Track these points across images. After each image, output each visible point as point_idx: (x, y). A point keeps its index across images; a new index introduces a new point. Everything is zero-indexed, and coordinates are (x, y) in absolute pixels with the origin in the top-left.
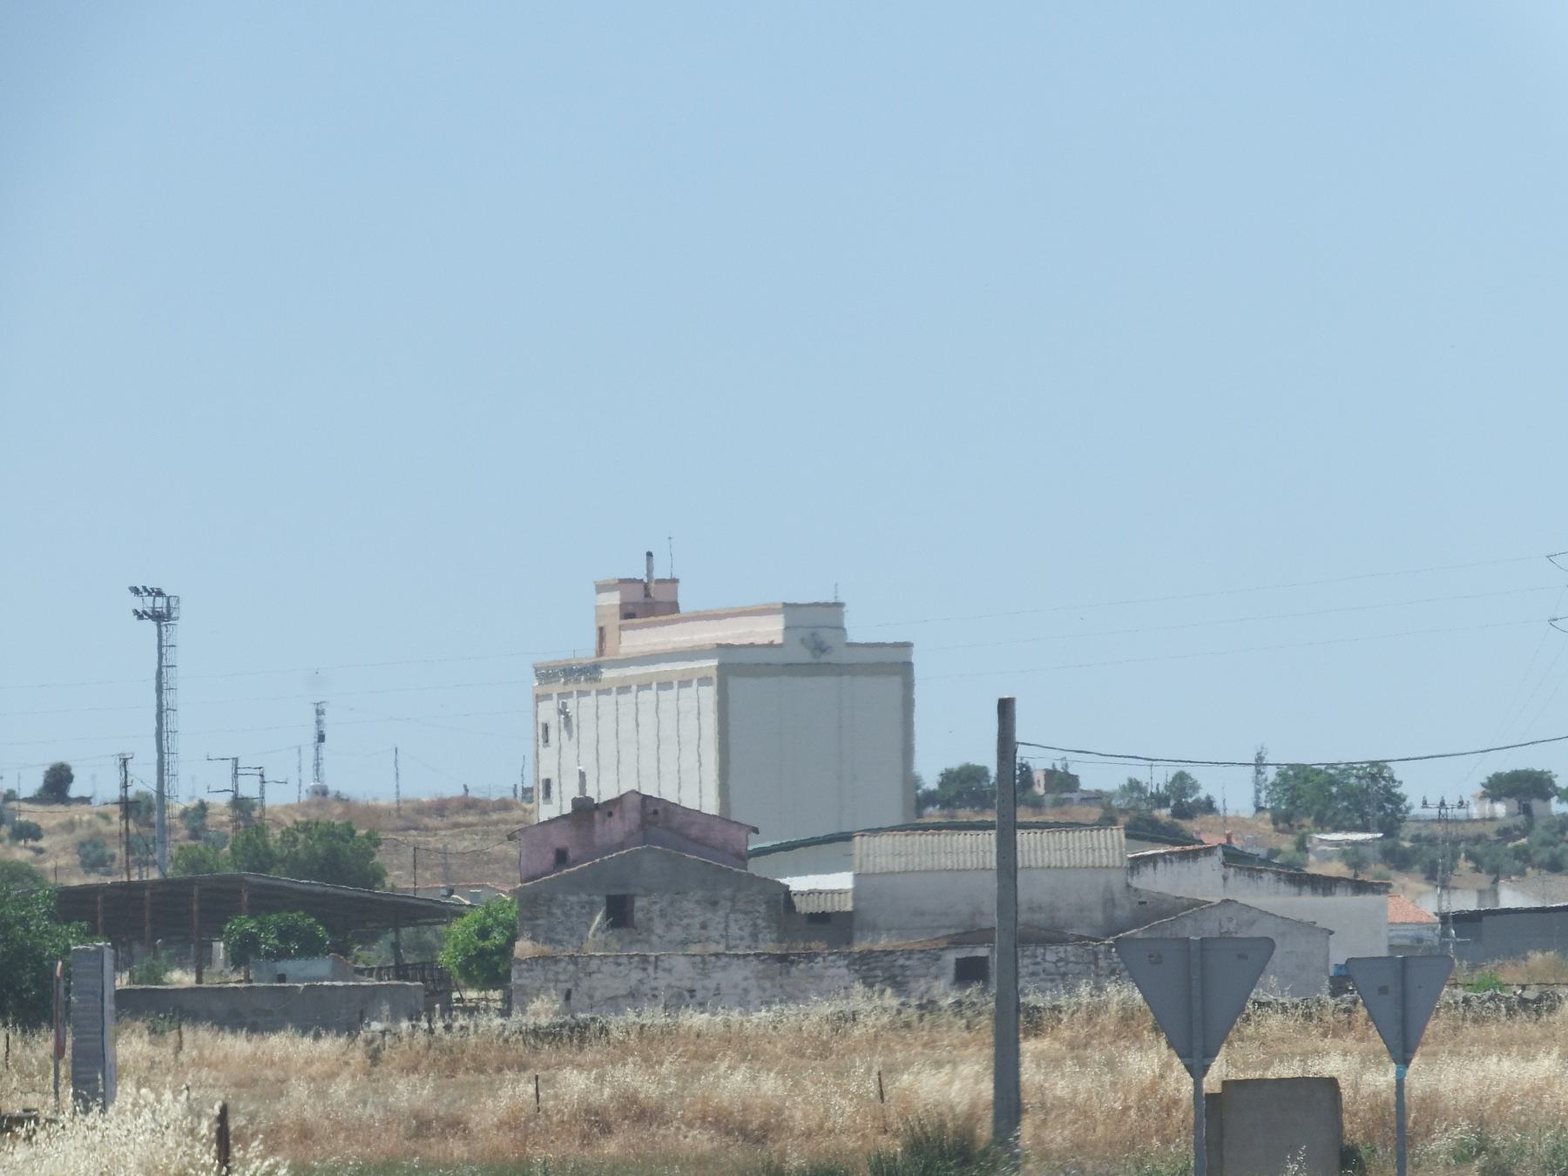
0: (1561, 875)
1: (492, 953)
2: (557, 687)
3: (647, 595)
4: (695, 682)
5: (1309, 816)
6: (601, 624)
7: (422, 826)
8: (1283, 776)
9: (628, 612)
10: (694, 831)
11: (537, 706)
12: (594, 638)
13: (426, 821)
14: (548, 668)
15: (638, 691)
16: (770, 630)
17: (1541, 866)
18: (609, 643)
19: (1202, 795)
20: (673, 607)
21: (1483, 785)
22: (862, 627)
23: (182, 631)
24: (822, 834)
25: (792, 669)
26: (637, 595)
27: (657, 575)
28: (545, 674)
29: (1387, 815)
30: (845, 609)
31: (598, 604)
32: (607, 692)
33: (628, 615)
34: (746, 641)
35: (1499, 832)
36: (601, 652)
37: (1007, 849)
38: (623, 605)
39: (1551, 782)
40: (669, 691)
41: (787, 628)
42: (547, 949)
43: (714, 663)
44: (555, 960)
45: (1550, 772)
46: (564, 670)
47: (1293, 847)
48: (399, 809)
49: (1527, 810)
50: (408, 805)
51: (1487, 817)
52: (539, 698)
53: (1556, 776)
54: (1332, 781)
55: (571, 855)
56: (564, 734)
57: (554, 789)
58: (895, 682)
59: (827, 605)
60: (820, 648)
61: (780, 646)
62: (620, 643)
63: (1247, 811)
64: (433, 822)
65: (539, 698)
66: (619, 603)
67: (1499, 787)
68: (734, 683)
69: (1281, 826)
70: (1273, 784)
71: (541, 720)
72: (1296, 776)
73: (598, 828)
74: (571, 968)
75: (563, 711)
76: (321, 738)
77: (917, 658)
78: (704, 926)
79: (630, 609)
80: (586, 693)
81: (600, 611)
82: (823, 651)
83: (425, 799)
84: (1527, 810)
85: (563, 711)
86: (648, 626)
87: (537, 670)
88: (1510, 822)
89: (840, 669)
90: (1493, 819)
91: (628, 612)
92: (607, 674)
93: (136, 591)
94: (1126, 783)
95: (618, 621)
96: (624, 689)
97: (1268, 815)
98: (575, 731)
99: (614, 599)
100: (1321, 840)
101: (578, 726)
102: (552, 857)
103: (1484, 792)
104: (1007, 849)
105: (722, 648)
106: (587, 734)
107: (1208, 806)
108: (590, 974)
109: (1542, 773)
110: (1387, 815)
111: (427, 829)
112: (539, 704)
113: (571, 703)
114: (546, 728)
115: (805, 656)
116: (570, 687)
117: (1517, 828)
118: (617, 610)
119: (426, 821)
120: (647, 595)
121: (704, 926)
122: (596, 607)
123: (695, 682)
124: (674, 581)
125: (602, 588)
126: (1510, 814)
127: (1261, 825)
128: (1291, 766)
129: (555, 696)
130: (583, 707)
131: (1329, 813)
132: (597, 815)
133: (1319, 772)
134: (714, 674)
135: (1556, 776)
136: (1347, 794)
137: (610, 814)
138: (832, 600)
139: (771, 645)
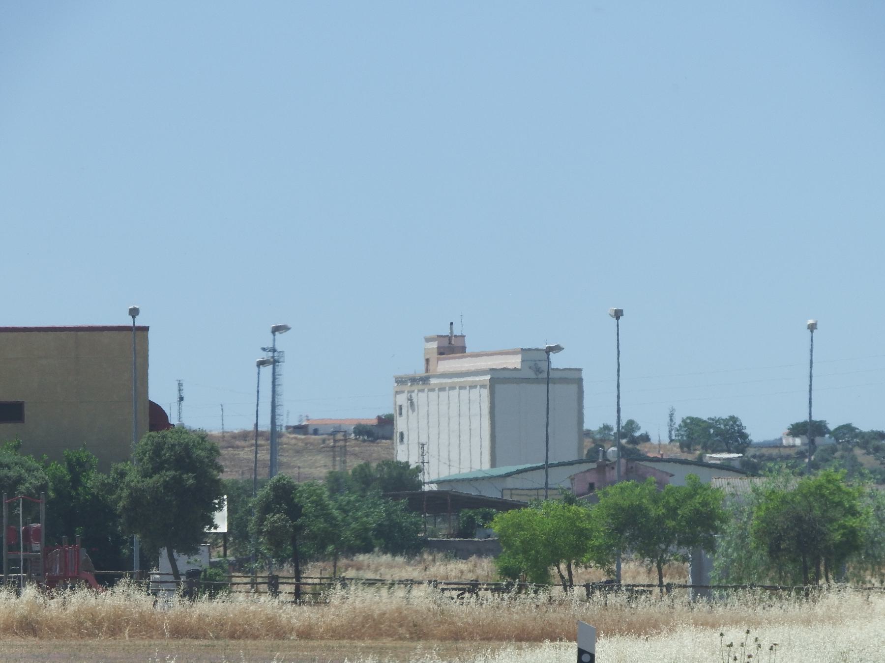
0: (232, 432)
3: (450, 343)
4: (479, 387)
5: (699, 444)
6: (427, 357)
7: (235, 446)
8: (684, 421)
11: (396, 396)
12: (423, 363)
13: (238, 443)
14: (401, 378)
15: (449, 390)
16: (515, 362)
18: (431, 367)
20: (463, 349)
21: (789, 429)
23: (284, 369)
25: (527, 380)
26: (446, 343)
28: (400, 381)
29: (739, 444)
30: (465, 338)
31: (426, 347)
32: (433, 390)
33: (441, 354)
35: (797, 453)
36: (427, 370)
37: (256, 442)
38: (439, 348)
39: (825, 427)
40: (455, 390)
43: (488, 377)
45: (826, 421)
47: (820, 470)
48: (224, 437)
49: (812, 442)
50: (229, 434)
51: (792, 445)
52: (397, 393)
53: (828, 423)
54: (710, 426)
56: (410, 411)
58: (574, 388)
62: (437, 366)
63: (666, 440)
64: (242, 443)
66: (436, 346)
67: (797, 430)
68: (498, 387)
69: (685, 449)
71: (399, 403)
72: (691, 423)
73: (607, 474)
75: (410, 400)
76: (181, 399)
77: (584, 375)
79: (442, 350)
80: (422, 391)
82: (540, 373)
83: (236, 431)
85: (410, 400)
86: (450, 358)
88: (803, 448)
90: (794, 446)
92: (433, 381)
93: (264, 349)
94: (602, 426)
95: (435, 355)
96: (442, 389)
98: (416, 409)
99: (434, 345)
100: (711, 457)
101: (418, 406)
102: (587, 486)
103: (790, 432)
104: (256, 442)
106: (423, 411)
107: (646, 438)
109: (821, 422)
110: (739, 444)
111: (238, 447)
112: (397, 395)
113: (414, 395)
114: (401, 407)
115: (531, 375)
118: (436, 351)
119: (238, 443)
120: (450, 343)
122: (425, 349)
123: (479, 387)
125: (428, 340)
126: (803, 444)
127: (675, 449)
128: (688, 418)
129: (406, 392)
130: (420, 398)
131: (709, 443)
132: (607, 468)
133: (705, 421)
134: (488, 383)
135: (828, 423)
136: (719, 433)
139: (515, 369)
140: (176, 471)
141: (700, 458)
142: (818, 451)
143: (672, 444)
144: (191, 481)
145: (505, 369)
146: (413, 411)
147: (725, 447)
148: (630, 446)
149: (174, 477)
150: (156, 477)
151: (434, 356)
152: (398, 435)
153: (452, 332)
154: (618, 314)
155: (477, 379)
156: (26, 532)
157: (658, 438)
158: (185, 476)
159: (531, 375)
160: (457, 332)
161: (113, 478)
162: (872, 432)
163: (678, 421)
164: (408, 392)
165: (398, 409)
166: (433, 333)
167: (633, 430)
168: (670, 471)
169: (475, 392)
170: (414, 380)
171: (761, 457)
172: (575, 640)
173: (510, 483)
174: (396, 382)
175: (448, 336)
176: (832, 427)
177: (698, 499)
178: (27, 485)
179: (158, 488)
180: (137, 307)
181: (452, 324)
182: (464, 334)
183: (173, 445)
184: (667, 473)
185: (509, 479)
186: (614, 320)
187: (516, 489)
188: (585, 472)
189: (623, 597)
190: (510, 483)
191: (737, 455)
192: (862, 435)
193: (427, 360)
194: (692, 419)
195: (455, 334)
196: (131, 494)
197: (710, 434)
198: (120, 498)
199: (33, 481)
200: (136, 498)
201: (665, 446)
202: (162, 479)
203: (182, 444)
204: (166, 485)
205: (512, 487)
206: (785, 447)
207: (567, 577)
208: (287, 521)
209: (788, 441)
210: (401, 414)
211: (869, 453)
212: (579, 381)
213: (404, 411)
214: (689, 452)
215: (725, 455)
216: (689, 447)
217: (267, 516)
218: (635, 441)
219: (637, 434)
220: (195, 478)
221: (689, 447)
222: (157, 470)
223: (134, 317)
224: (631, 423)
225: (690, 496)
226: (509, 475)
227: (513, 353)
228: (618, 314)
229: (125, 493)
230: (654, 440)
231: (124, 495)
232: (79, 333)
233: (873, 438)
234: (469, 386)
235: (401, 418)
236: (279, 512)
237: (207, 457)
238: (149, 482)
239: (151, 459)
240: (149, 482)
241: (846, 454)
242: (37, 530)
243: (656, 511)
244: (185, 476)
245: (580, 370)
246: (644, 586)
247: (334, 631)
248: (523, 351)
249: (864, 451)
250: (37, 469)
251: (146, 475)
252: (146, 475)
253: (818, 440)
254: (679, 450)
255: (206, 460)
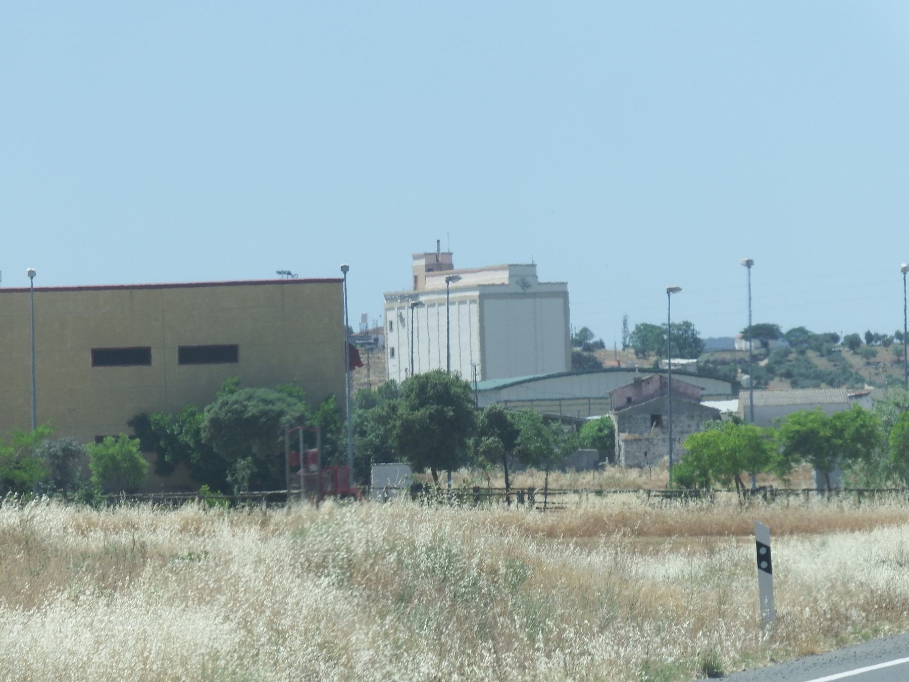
1: (603, 438)
2: (397, 304)
6: (416, 274)
8: (638, 328)
9: (429, 269)
10: (681, 390)
16: (502, 277)
17: (781, 375)
19: (596, 339)
22: (545, 275)
24: (555, 373)
27: (442, 251)
28: (390, 298)
34: (491, 282)
36: (415, 289)
38: (426, 266)
41: (510, 276)
42: (637, 436)
43: (477, 293)
44: (640, 440)
46: (401, 296)
49: (765, 345)
52: (387, 310)
55: (633, 400)
56: (400, 327)
57: (396, 352)
58: (560, 301)
59: (528, 265)
60: (525, 285)
61: (508, 285)
65: (387, 310)
68: (487, 302)
69: (640, 355)
70: (633, 333)
73: (644, 389)
74: (647, 443)
77: (570, 289)
78: (689, 426)
79: (430, 267)
81: (415, 268)
82: (528, 287)
84: (765, 345)
87: (385, 296)
89: (535, 295)
91: (429, 269)
96: (432, 305)
97: (632, 351)
99: (422, 262)
102: (626, 400)
105: (481, 287)
107: (601, 345)
108: (654, 446)
114: (391, 323)
115: (519, 289)
116: (403, 304)
117: (761, 355)
118: (424, 268)
120: (437, 260)
121: (689, 426)
124: (451, 254)
125: (416, 257)
128: (642, 325)
129: (396, 309)
132: (643, 383)
137: (648, 383)
138: (530, 262)
139: (503, 284)
140: (438, 405)
141: (656, 364)
142: (772, 355)
143: (626, 349)
144: (451, 413)
145: (493, 285)
146: (404, 326)
147: (678, 352)
148: (585, 354)
149: (437, 410)
150: (422, 411)
151: (422, 273)
152: (389, 350)
153: (439, 250)
154: (749, 264)
155: (468, 294)
156: (305, 455)
157: (613, 345)
158: (445, 409)
159: (519, 289)
160: (443, 250)
161: (387, 412)
162: (825, 335)
163: (632, 328)
164: (399, 308)
165: (388, 323)
166: (422, 251)
167: (586, 338)
168: (701, 386)
169: (464, 308)
170: (403, 297)
171: (714, 362)
172: (753, 534)
173: (505, 395)
174: (386, 299)
175: (435, 254)
176: (784, 330)
177: (859, 422)
178: (288, 417)
179: (425, 419)
180: (347, 264)
181: (438, 241)
182: (451, 251)
183: (436, 385)
184: (698, 387)
185: (504, 391)
186: (746, 268)
187: (539, 400)
188: (624, 387)
189: (802, 497)
190: (505, 395)
191: (691, 361)
192: (816, 338)
193: (416, 278)
194: (646, 326)
195: (442, 251)
196: (403, 424)
197: (664, 340)
198: (394, 426)
199: (293, 413)
200: (408, 427)
201: (620, 353)
202: (428, 411)
203: (442, 383)
204: (431, 417)
205: (506, 399)
206: (738, 351)
207: (739, 483)
208: (499, 443)
209: (742, 345)
210: (391, 329)
211: (822, 356)
212: (564, 295)
213: (395, 327)
214: (645, 357)
215: (684, 361)
216: (643, 352)
217: (483, 438)
218: (589, 348)
219: (591, 341)
220: (454, 411)
221: (643, 352)
222: (422, 405)
223: (345, 273)
224: (585, 332)
225: (854, 420)
226: (505, 387)
227: (502, 268)
228: (749, 264)
229: (398, 423)
230: (609, 346)
231: (397, 425)
232: (285, 286)
233: (827, 341)
234: (470, 301)
235: (392, 333)
236: (492, 435)
237: (463, 393)
238: (419, 414)
239: (418, 396)
240: (419, 414)
241: (800, 357)
242: (314, 455)
243: (826, 432)
244: (445, 409)
245: (564, 284)
246: (499, 489)
247: (572, 530)
248: (511, 267)
249: (818, 353)
250: (295, 404)
251: (414, 408)
252: (414, 408)
253: (772, 343)
254: (635, 356)
255: (463, 396)
